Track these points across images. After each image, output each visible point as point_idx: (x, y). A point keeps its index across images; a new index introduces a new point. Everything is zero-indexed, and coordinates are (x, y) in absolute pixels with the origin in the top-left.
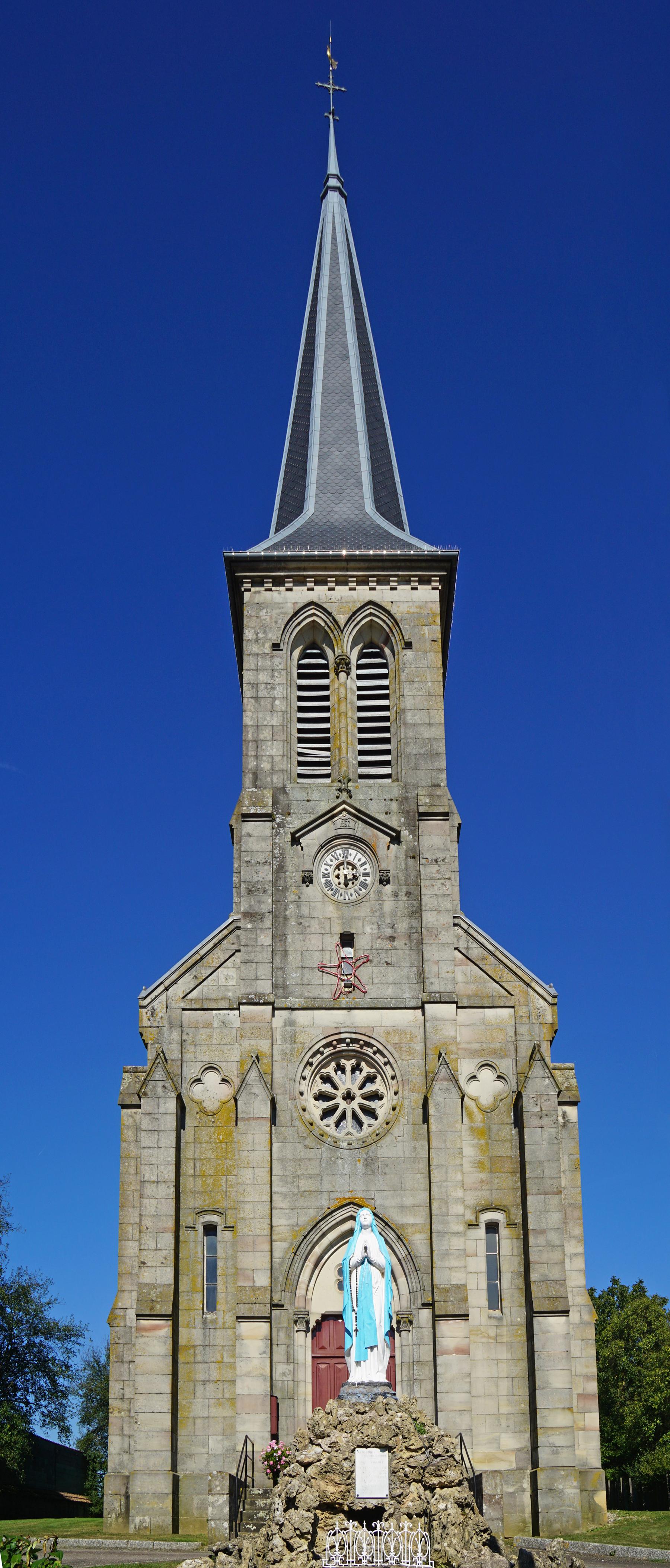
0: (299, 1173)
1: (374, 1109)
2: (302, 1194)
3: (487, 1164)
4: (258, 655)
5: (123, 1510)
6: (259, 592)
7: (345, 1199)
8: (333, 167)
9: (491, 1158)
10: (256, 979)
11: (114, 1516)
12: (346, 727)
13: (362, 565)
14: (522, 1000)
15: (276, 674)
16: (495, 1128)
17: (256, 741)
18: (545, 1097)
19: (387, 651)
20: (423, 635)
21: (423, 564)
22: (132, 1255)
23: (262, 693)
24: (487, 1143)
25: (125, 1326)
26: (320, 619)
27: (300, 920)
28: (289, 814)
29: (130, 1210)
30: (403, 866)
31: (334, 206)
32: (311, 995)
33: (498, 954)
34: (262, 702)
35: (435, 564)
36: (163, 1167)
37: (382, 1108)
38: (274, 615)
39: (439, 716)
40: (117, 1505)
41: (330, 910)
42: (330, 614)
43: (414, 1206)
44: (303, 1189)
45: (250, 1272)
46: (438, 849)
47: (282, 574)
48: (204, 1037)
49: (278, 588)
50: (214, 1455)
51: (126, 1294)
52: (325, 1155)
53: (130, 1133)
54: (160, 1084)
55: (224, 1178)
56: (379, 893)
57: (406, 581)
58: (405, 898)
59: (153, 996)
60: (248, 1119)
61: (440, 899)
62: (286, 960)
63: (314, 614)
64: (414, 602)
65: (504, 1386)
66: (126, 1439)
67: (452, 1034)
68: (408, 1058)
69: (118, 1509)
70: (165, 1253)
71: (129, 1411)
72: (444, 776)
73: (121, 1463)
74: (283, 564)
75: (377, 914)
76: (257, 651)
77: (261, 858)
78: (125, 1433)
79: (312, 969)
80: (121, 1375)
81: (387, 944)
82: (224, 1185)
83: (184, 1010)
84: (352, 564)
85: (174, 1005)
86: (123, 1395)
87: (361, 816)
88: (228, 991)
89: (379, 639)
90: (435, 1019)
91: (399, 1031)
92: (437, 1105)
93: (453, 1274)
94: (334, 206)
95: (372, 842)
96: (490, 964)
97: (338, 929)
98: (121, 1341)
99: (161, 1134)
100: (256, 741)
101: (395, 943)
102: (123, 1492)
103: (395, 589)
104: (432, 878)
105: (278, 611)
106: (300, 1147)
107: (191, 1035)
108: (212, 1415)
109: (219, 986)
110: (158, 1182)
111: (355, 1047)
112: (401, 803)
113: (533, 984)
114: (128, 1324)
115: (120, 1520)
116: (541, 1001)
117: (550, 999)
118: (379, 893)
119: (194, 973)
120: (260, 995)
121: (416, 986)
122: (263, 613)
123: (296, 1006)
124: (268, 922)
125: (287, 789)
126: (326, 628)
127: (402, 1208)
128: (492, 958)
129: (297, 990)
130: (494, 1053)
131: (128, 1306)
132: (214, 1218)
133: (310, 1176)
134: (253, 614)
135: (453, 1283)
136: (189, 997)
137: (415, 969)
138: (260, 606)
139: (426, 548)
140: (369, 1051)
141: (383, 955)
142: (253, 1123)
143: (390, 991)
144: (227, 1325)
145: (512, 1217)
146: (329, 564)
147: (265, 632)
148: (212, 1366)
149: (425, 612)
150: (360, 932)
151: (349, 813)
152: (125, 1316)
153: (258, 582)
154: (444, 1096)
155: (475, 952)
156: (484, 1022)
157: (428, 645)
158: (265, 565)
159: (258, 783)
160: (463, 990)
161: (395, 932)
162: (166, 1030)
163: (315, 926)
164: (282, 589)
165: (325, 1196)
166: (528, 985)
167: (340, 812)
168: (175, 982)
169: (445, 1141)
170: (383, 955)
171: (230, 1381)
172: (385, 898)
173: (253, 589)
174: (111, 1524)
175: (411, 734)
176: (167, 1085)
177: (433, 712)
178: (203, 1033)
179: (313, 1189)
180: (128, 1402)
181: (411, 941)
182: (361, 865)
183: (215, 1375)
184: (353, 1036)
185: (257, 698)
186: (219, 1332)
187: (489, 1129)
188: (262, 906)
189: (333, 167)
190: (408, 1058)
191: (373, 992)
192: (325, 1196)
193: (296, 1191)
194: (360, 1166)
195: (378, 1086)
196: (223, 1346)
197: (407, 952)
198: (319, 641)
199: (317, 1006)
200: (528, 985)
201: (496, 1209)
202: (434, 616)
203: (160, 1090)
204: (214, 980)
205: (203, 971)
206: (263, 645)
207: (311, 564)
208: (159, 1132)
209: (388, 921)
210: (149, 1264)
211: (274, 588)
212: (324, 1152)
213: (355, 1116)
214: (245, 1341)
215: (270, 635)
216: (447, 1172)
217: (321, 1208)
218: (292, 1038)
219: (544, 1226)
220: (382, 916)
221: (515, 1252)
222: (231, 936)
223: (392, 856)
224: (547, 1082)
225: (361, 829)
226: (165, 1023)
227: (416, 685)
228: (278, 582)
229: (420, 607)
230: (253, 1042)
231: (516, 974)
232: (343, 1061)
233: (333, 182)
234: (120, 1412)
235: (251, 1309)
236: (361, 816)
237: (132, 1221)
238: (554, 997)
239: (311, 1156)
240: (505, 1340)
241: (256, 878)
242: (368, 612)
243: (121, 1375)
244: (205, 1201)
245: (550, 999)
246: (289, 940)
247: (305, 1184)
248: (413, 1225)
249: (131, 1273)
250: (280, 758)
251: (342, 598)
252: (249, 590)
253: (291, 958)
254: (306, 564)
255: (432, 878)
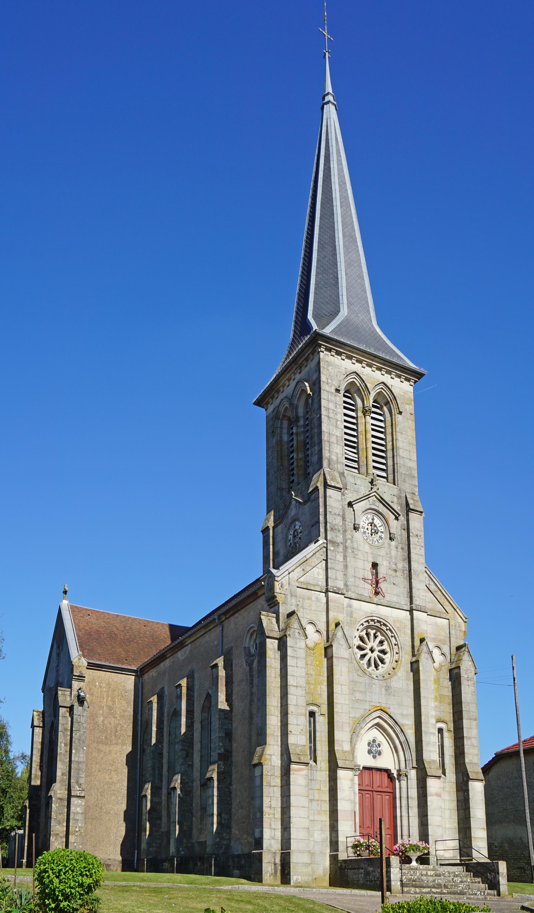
0: (355, 689)
1: (384, 659)
2: (357, 701)
3: (438, 699)
4: (328, 392)
5: (273, 872)
6: (328, 355)
7: (377, 707)
8: (329, 88)
9: (440, 695)
10: (336, 579)
11: (268, 875)
12: (367, 444)
13: (381, 361)
14: (452, 617)
15: (338, 406)
16: (441, 680)
17: (329, 442)
18: (470, 671)
19: (385, 408)
20: (406, 409)
21: (409, 372)
22: (274, 724)
23: (331, 415)
24: (438, 687)
25: (271, 765)
26: (358, 382)
27: (353, 550)
28: (346, 489)
29: (273, 698)
30: (400, 533)
31: (331, 113)
32: (359, 593)
33: (442, 591)
34: (331, 420)
35: (414, 374)
36: (299, 678)
37: (387, 658)
38: (336, 372)
39: (414, 457)
40: (270, 869)
41: (367, 548)
42: (364, 382)
43: (407, 715)
44: (357, 698)
45: (340, 742)
46: (418, 530)
47: (342, 351)
48: (308, 605)
49: (337, 356)
50: (317, 842)
51: (271, 746)
52: (367, 681)
53: (271, 653)
54: (297, 631)
55: (319, 686)
56: (389, 544)
57: (399, 377)
58: (401, 551)
59: (282, 576)
60: (338, 658)
61: (419, 557)
62: (347, 571)
63: (355, 378)
64: (403, 388)
65: (447, 813)
66: (273, 831)
67: (425, 629)
68: (403, 636)
69: (270, 871)
70: (301, 727)
71: (274, 814)
72: (417, 489)
73: (270, 845)
74: (343, 346)
75: (389, 556)
76: (328, 390)
77: (337, 512)
78: (272, 827)
79: (359, 578)
80: (269, 793)
81: (393, 573)
82: (319, 690)
83: (298, 587)
84: (376, 359)
85: (292, 583)
86: (271, 805)
87: (381, 500)
88: (319, 581)
89: (385, 401)
90: (418, 619)
91: (396, 620)
92: (423, 665)
93: (431, 754)
94: (331, 113)
95: (386, 517)
96: (439, 595)
97: (371, 560)
98: (269, 774)
99: (298, 659)
100: (329, 442)
101: (397, 574)
102: (273, 861)
103: (393, 379)
104: (415, 544)
105: (338, 370)
106: (355, 675)
107: (301, 602)
108: (316, 819)
109: (315, 578)
110: (297, 686)
111: (378, 624)
112: (398, 499)
113: (457, 610)
114: (273, 764)
115: (272, 877)
116: (460, 619)
117: (464, 619)
118: (389, 544)
119: (303, 568)
120: (339, 589)
121: (406, 599)
122: (330, 368)
123: (353, 598)
124: (341, 549)
125: (345, 475)
126: (360, 387)
127: (402, 715)
128: (439, 592)
129: (353, 588)
130: (441, 641)
131: (273, 754)
132: (315, 708)
133: (361, 692)
134: (325, 367)
135: (432, 759)
136: (300, 580)
137: (406, 589)
138: (329, 363)
139: (411, 365)
140: (384, 628)
141: (392, 579)
142: (341, 660)
143: (395, 599)
144: (322, 769)
145: (449, 727)
146: (366, 355)
147: (331, 380)
148: (315, 791)
149: (407, 397)
150: (381, 563)
151: (376, 497)
152: (271, 759)
153: (329, 350)
154: (426, 661)
155: (433, 587)
156: (436, 624)
157: (409, 415)
158: (334, 343)
159: (331, 466)
160: (429, 606)
161: (397, 568)
162: (289, 596)
163: (360, 555)
164: (339, 357)
165: (368, 703)
166: (455, 609)
167: (372, 496)
168: (293, 571)
169: (427, 685)
170: (392, 579)
171: (324, 801)
172: (392, 548)
173: (325, 352)
174: (267, 879)
175: (402, 462)
176: (300, 632)
177: (412, 453)
178: (307, 602)
179: (362, 699)
180: (273, 809)
181: (404, 574)
182: (380, 526)
183: (317, 797)
184: (379, 619)
185: (328, 417)
186: (318, 773)
187: (439, 680)
188: (338, 539)
189: (329, 88)
190: (403, 636)
191: (388, 597)
192: (368, 703)
193: (354, 699)
194: (383, 690)
195: (385, 647)
196: (321, 781)
197: (402, 579)
198: (352, 391)
199: (363, 599)
200: (455, 609)
201: (443, 722)
202: (411, 400)
203: (297, 634)
204: (312, 573)
205: (307, 568)
206: (331, 387)
207: (357, 352)
208: (297, 658)
209: (394, 561)
210: (293, 732)
211: (335, 356)
212: (366, 679)
213: (369, 660)
214: (342, 781)
215: (334, 383)
216: (428, 701)
217: (365, 710)
218: (351, 614)
219: (470, 735)
220: (391, 557)
221: (451, 746)
222: (320, 551)
223: (396, 526)
224: (470, 663)
225: (381, 508)
226: (288, 593)
227: (404, 436)
228: (339, 353)
229: (404, 393)
230: (335, 614)
231: (450, 603)
232: (378, 634)
233: (330, 98)
234: (269, 815)
235: (345, 763)
236: (381, 500)
237: (273, 705)
238: (466, 618)
239: (361, 681)
240: (447, 790)
241: (334, 523)
242: (381, 387)
243: (269, 793)
244: (310, 698)
245: (464, 619)
246: (348, 560)
247: (358, 696)
248: (407, 725)
249: (274, 735)
250: (341, 455)
251: (373, 376)
252: (323, 352)
253: (349, 570)
254: (355, 351)
255: (415, 544)
